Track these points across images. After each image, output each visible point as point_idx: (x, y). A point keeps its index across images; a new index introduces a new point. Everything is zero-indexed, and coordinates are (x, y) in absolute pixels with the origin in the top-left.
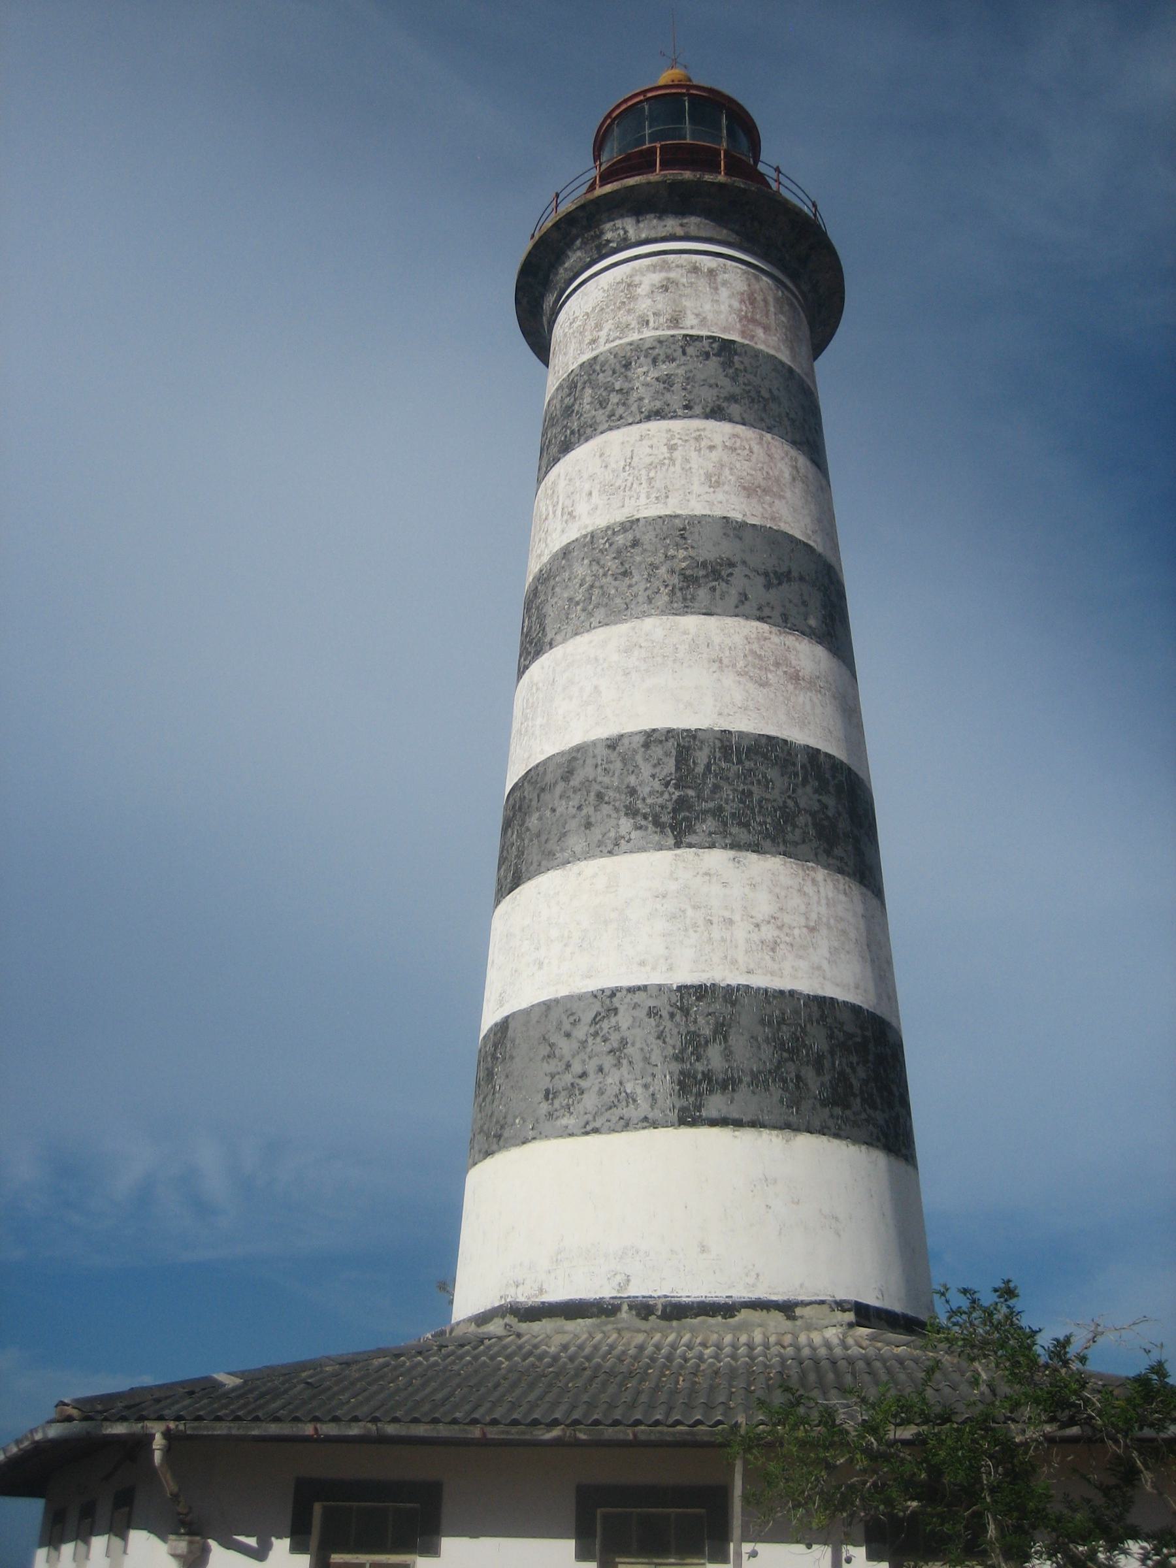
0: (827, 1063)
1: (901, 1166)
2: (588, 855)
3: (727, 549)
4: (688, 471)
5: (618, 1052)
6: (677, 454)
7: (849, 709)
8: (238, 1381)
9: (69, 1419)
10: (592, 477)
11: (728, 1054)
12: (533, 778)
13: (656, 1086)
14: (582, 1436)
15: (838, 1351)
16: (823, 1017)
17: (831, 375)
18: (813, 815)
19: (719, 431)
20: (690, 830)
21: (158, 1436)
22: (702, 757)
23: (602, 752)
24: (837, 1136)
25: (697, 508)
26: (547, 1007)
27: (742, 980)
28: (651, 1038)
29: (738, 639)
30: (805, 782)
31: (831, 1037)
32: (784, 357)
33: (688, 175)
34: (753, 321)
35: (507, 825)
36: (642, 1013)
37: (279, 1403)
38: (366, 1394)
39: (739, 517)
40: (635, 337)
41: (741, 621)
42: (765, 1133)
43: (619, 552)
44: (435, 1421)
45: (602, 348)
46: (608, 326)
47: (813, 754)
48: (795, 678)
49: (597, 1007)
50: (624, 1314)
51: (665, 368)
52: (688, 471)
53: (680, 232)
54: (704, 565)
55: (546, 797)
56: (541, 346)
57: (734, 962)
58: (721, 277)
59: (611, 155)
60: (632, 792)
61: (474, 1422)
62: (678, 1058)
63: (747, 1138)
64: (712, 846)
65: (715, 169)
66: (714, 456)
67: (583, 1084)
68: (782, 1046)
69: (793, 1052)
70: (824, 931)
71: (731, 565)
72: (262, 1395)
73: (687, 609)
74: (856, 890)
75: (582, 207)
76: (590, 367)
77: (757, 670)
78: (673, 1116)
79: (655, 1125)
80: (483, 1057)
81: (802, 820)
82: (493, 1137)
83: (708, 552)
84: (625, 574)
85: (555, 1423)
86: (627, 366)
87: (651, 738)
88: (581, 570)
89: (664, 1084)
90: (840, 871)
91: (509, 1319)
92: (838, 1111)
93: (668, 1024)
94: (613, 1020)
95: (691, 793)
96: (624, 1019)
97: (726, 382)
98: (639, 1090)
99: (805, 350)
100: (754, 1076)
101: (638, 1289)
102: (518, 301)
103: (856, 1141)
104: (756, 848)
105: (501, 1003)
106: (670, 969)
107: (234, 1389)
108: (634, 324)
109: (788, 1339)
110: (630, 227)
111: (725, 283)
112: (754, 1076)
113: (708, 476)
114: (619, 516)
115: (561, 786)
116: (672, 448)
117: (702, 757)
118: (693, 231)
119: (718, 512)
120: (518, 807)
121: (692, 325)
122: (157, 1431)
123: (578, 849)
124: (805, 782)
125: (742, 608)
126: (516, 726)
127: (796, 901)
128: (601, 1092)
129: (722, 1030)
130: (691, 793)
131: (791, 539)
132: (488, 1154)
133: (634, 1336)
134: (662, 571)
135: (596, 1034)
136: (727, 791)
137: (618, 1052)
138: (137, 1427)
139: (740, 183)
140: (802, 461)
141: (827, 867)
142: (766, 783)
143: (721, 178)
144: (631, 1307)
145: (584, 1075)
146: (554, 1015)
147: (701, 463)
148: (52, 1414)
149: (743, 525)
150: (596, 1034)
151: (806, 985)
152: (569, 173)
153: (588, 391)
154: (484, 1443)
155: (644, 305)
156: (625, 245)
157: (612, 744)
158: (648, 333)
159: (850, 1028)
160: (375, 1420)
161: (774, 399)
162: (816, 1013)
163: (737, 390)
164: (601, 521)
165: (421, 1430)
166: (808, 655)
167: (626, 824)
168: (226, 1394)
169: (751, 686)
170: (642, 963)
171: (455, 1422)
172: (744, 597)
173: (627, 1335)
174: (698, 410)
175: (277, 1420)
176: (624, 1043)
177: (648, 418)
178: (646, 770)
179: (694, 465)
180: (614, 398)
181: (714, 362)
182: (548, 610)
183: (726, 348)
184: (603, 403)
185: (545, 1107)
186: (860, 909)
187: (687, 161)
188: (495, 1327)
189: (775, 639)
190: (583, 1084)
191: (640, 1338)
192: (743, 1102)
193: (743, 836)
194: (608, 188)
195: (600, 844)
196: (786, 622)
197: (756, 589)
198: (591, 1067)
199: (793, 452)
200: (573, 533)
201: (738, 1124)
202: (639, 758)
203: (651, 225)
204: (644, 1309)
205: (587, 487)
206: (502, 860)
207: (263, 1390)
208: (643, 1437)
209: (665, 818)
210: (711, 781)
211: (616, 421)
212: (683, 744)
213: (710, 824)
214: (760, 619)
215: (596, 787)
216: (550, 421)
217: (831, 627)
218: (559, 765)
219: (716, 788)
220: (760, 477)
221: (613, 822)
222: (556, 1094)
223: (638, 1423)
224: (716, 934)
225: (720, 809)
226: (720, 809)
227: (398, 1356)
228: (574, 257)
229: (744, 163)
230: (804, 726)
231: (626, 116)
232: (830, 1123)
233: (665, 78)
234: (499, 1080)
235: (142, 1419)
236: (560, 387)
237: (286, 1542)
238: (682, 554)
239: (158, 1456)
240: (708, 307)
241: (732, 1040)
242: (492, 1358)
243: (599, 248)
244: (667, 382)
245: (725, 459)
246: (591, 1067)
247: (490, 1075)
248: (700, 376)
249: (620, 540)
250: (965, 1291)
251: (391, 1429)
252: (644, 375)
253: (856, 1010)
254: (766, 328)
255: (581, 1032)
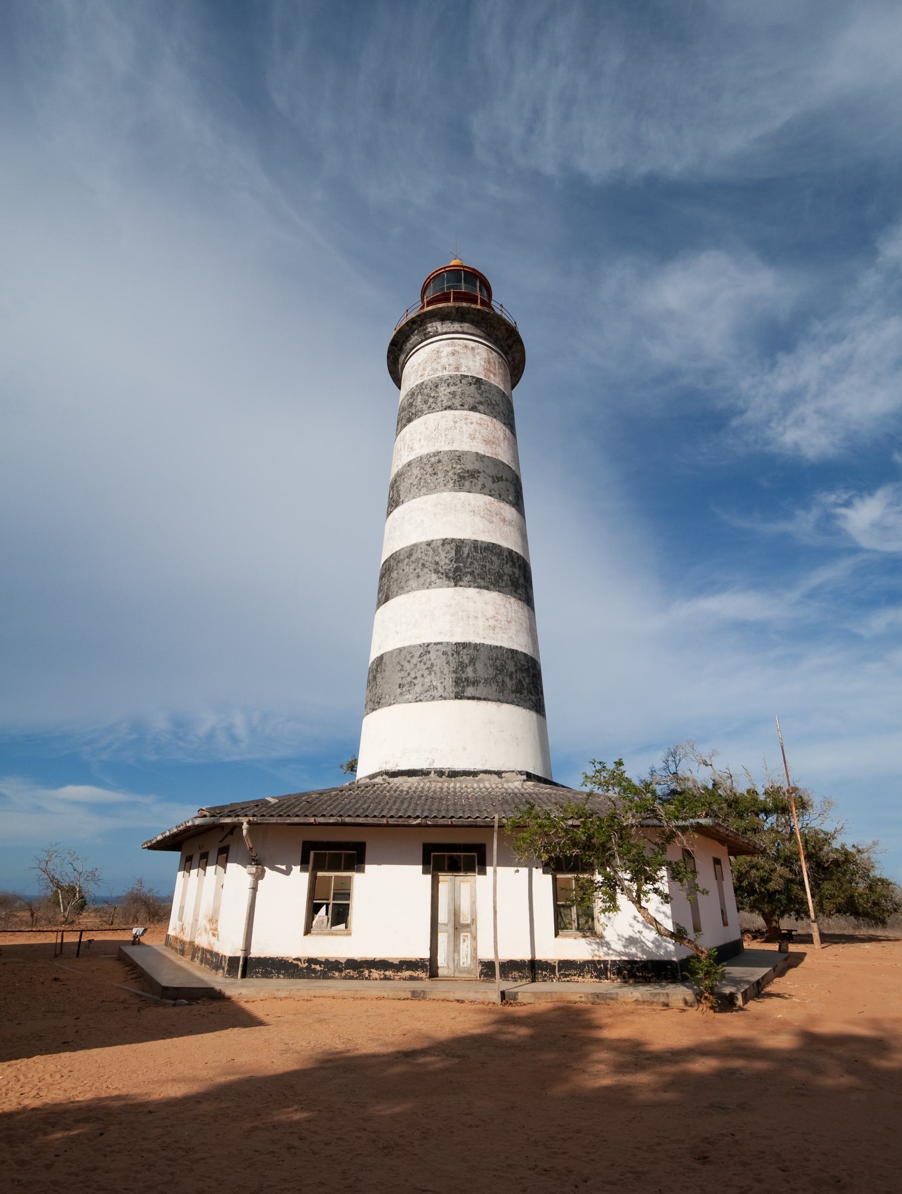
0: (514, 676)
1: (541, 717)
2: (418, 589)
3: (477, 466)
4: (461, 432)
5: (430, 669)
6: (457, 425)
7: (524, 536)
8: (276, 801)
9: (205, 816)
10: (421, 433)
11: (475, 671)
12: (395, 558)
13: (446, 683)
14: (429, 823)
15: (523, 790)
16: (513, 657)
17: (518, 396)
18: (510, 576)
19: (475, 416)
20: (461, 580)
21: (245, 824)
22: (466, 550)
23: (424, 547)
24: (518, 705)
25: (466, 448)
26: (400, 650)
27: (482, 641)
28: (444, 664)
29: (481, 503)
30: (507, 563)
31: (516, 665)
32: (501, 387)
33: (464, 304)
34: (489, 371)
35: (382, 576)
36: (440, 653)
37: (296, 810)
38: (340, 806)
39: (482, 453)
40: (440, 374)
41: (483, 496)
42: (490, 703)
43: (432, 465)
44: (367, 816)
45: (426, 378)
46: (429, 369)
47: (510, 552)
48: (504, 520)
49: (421, 650)
50: (432, 775)
51: (453, 388)
52: (461, 432)
53: (460, 330)
54: (468, 471)
55: (400, 565)
56: (397, 379)
57: (478, 634)
58: (476, 351)
59: (430, 294)
60: (437, 563)
61: (383, 817)
62: (455, 672)
63: (482, 704)
64: (470, 587)
65: (476, 303)
66: (473, 426)
67: (415, 681)
68: (497, 668)
69: (501, 671)
70: (514, 623)
71: (479, 472)
72: (288, 806)
73: (460, 489)
74: (526, 607)
75: (419, 316)
76: (421, 386)
77: (489, 516)
78: (453, 695)
79: (445, 698)
80: (371, 670)
81: (505, 578)
82: (376, 703)
83: (469, 467)
84: (435, 474)
85: (418, 817)
86: (437, 387)
87: (445, 542)
88: (416, 471)
89: (449, 682)
90: (520, 599)
91: (385, 777)
92: (518, 695)
93: (451, 658)
94: (428, 656)
95: (461, 565)
96: (433, 655)
97: (477, 396)
98: (439, 684)
99: (509, 386)
100: (486, 680)
101: (438, 765)
102: (388, 358)
103: (525, 707)
104: (487, 588)
105: (380, 649)
106: (452, 636)
107: (275, 804)
108: (440, 369)
109: (500, 786)
110: (438, 326)
111: (478, 354)
112: (486, 680)
113: (470, 435)
114: (433, 450)
115: (406, 561)
116: (455, 422)
117: (466, 550)
118: (466, 330)
119: (474, 450)
120: (387, 569)
121: (464, 371)
122: (244, 820)
123: (414, 586)
124: (507, 563)
125: (483, 490)
126: (386, 536)
127: (503, 610)
128: (423, 685)
129: (473, 661)
130: (461, 565)
131: (503, 463)
132: (373, 710)
133: (434, 784)
134: (450, 473)
135: (421, 661)
136: (476, 565)
137: (430, 669)
138: (235, 820)
139: (486, 310)
140: (508, 432)
141: (515, 597)
142: (492, 562)
143: (479, 307)
144: (435, 772)
145: (416, 678)
146: (403, 653)
147: (468, 429)
148: (197, 814)
149: (484, 456)
150: (421, 661)
151: (507, 645)
152: (409, 305)
153: (420, 397)
154: (388, 825)
155: (444, 361)
156: (437, 334)
157: (429, 544)
158: (446, 373)
159: (523, 662)
160: (341, 816)
161: (497, 404)
162: (510, 656)
163: (483, 400)
164: (424, 451)
165: (361, 820)
166: (509, 511)
167: (434, 576)
168: (272, 806)
169: (486, 523)
170: (441, 633)
171: (375, 816)
172: (484, 486)
173: (434, 784)
174: (466, 407)
175: (297, 816)
176: (432, 665)
177: (445, 409)
178: (443, 555)
179: (464, 430)
180: (431, 400)
181: (473, 387)
182: (401, 488)
183: (478, 381)
184: (426, 402)
185: (399, 691)
186: (527, 615)
187: (462, 299)
188: (379, 780)
189: (496, 504)
190: (415, 681)
191: (440, 785)
192: (481, 690)
193: (482, 583)
194: (430, 308)
195: (423, 584)
196: (500, 497)
197: (489, 484)
198: (419, 675)
199: (504, 428)
200: (412, 456)
201: (479, 699)
202: (440, 550)
203: (448, 326)
204: (440, 773)
205: (419, 437)
206: (380, 591)
207: (287, 805)
208: (455, 823)
209: (451, 575)
210: (469, 560)
211: (431, 410)
212: (459, 545)
213: (469, 578)
214: (490, 495)
215: (422, 561)
216: (403, 409)
217: (518, 503)
218: (406, 552)
219: (472, 563)
220: (491, 436)
221: (428, 575)
222: (404, 686)
223: (452, 817)
224: (471, 621)
225: (473, 572)
226: (473, 572)
227: (342, 791)
228: (414, 339)
229: (487, 303)
230: (508, 541)
231: (436, 277)
232: (515, 700)
233: (453, 263)
234: (379, 680)
235: (238, 816)
236: (407, 395)
237: (299, 867)
238: (459, 466)
239: (245, 832)
240: (471, 363)
241: (477, 665)
242: (381, 792)
243: (425, 335)
244: (454, 394)
245: (477, 428)
246: (419, 675)
247: (375, 678)
248: (467, 393)
249: (433, 460)
250: (600, 763)
251: (348, 820)
252: (443, 390)
253: (525, 655)
254: (494, 375)
255: (414, 661)
